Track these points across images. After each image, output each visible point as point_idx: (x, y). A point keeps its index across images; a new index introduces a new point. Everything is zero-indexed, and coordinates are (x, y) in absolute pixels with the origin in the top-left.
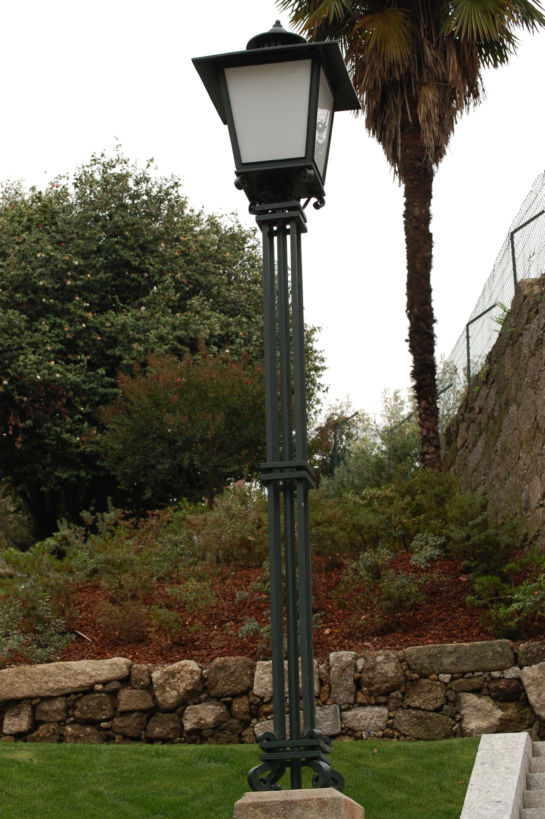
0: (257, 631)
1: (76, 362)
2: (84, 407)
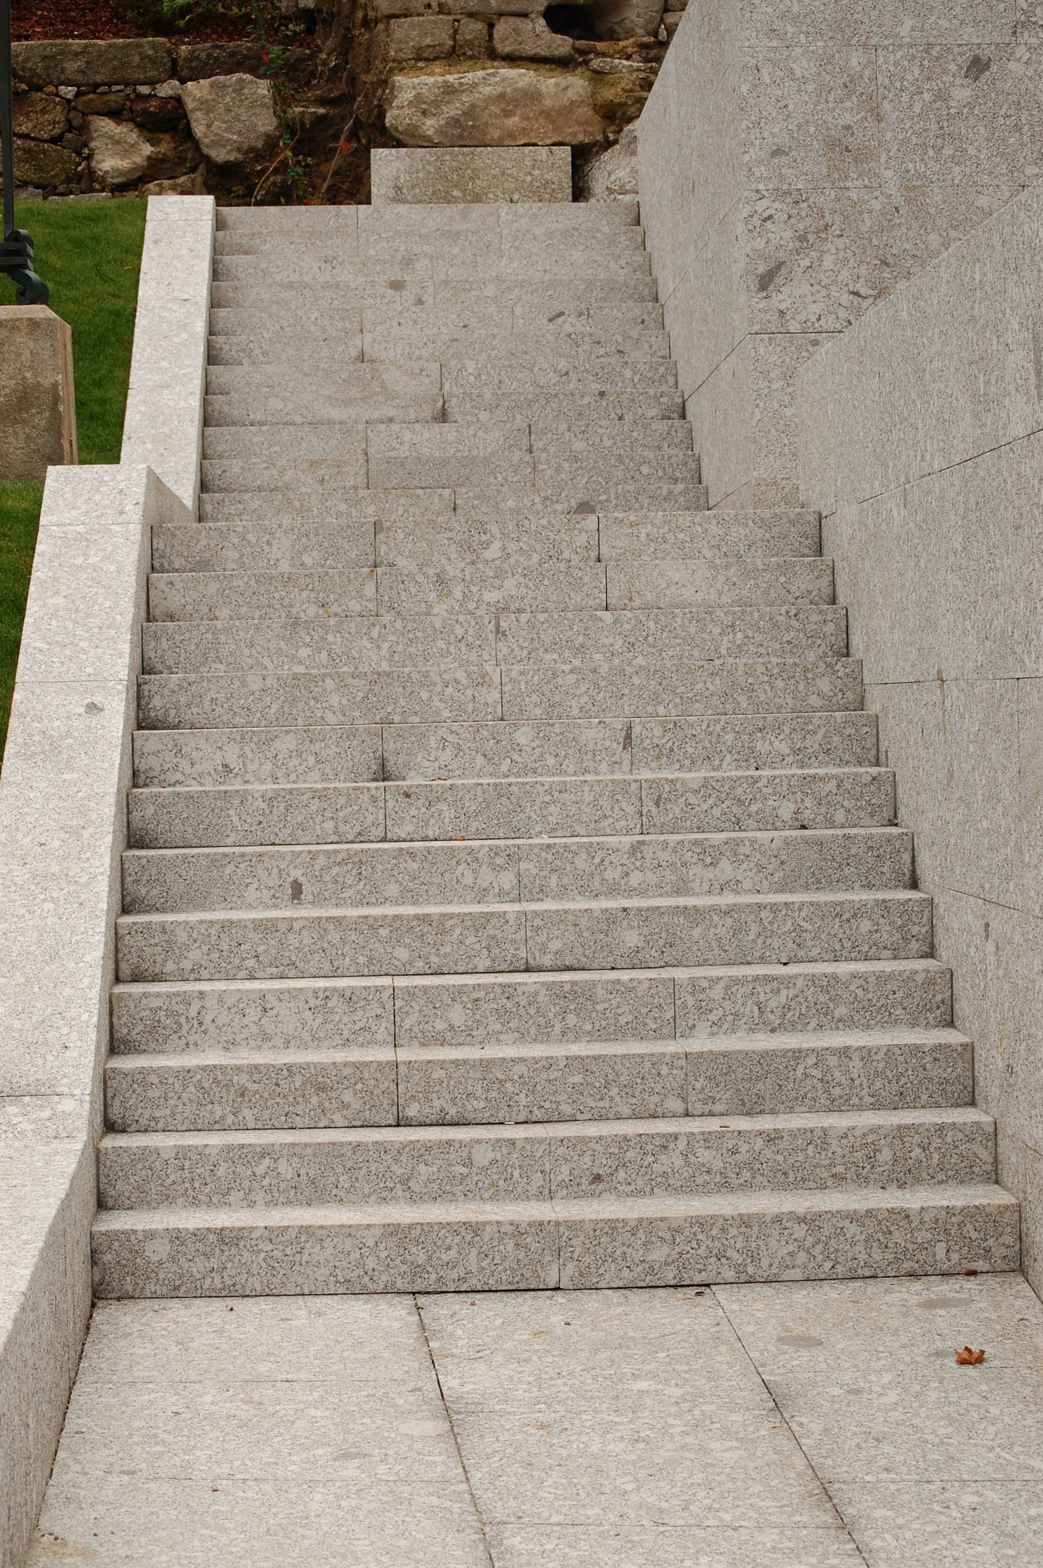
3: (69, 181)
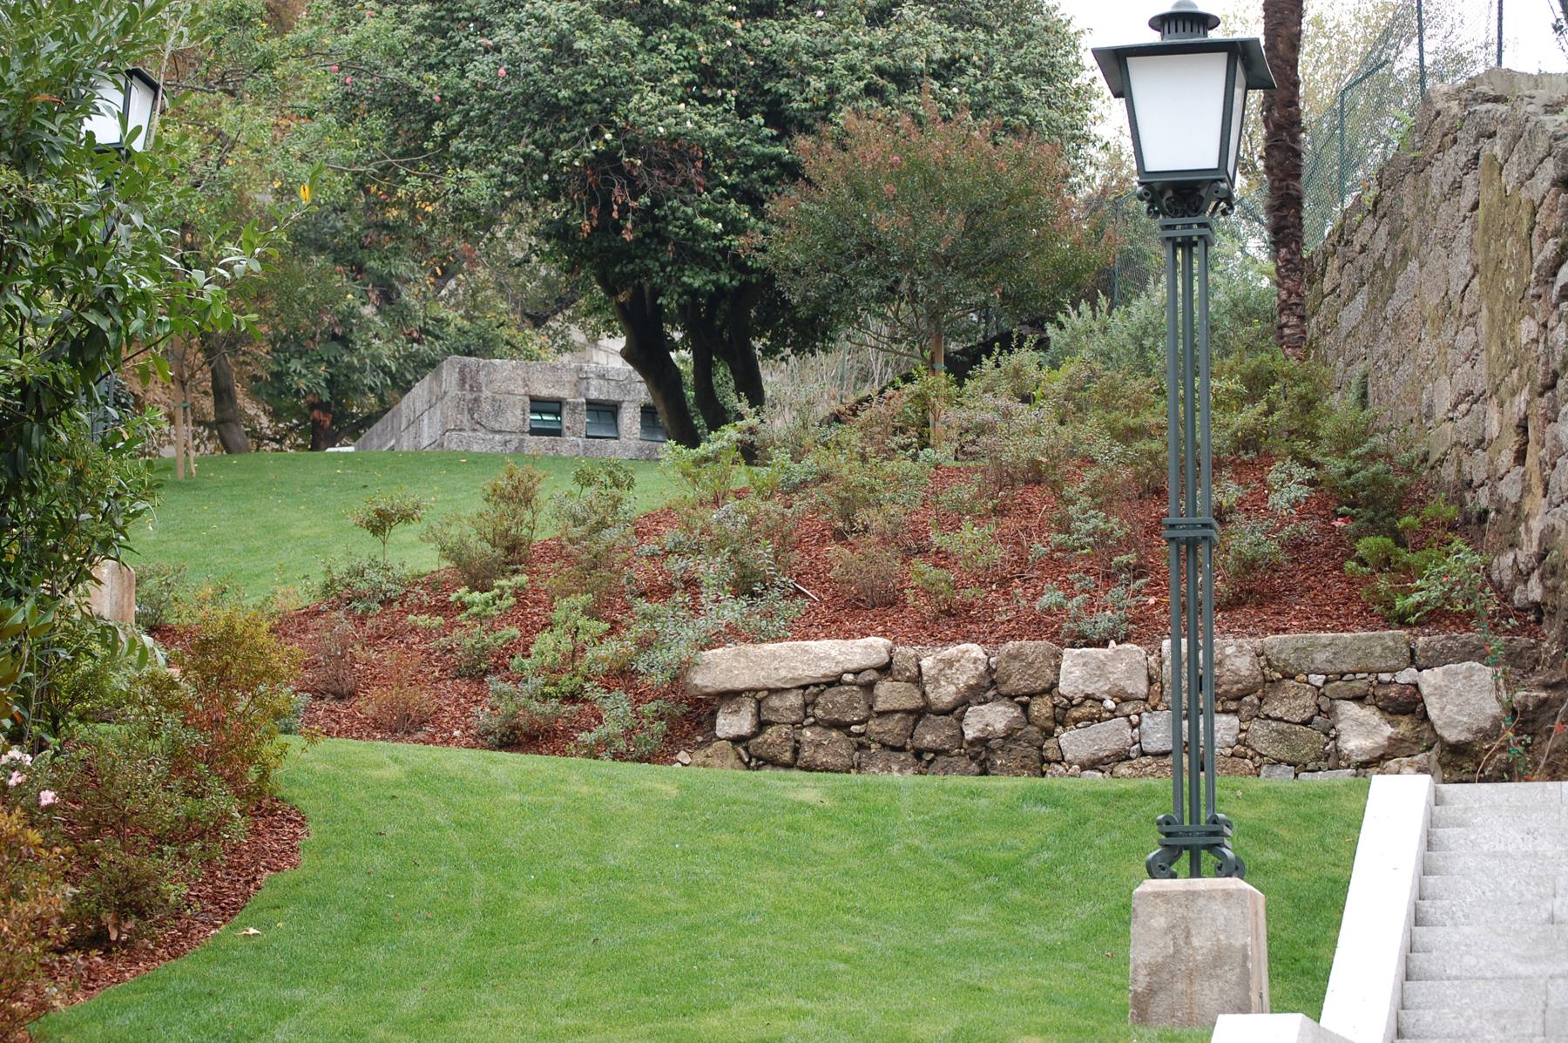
0: (1060, 607)
1: (717, 101)
2: (729, 175)
3: (1318, 759)
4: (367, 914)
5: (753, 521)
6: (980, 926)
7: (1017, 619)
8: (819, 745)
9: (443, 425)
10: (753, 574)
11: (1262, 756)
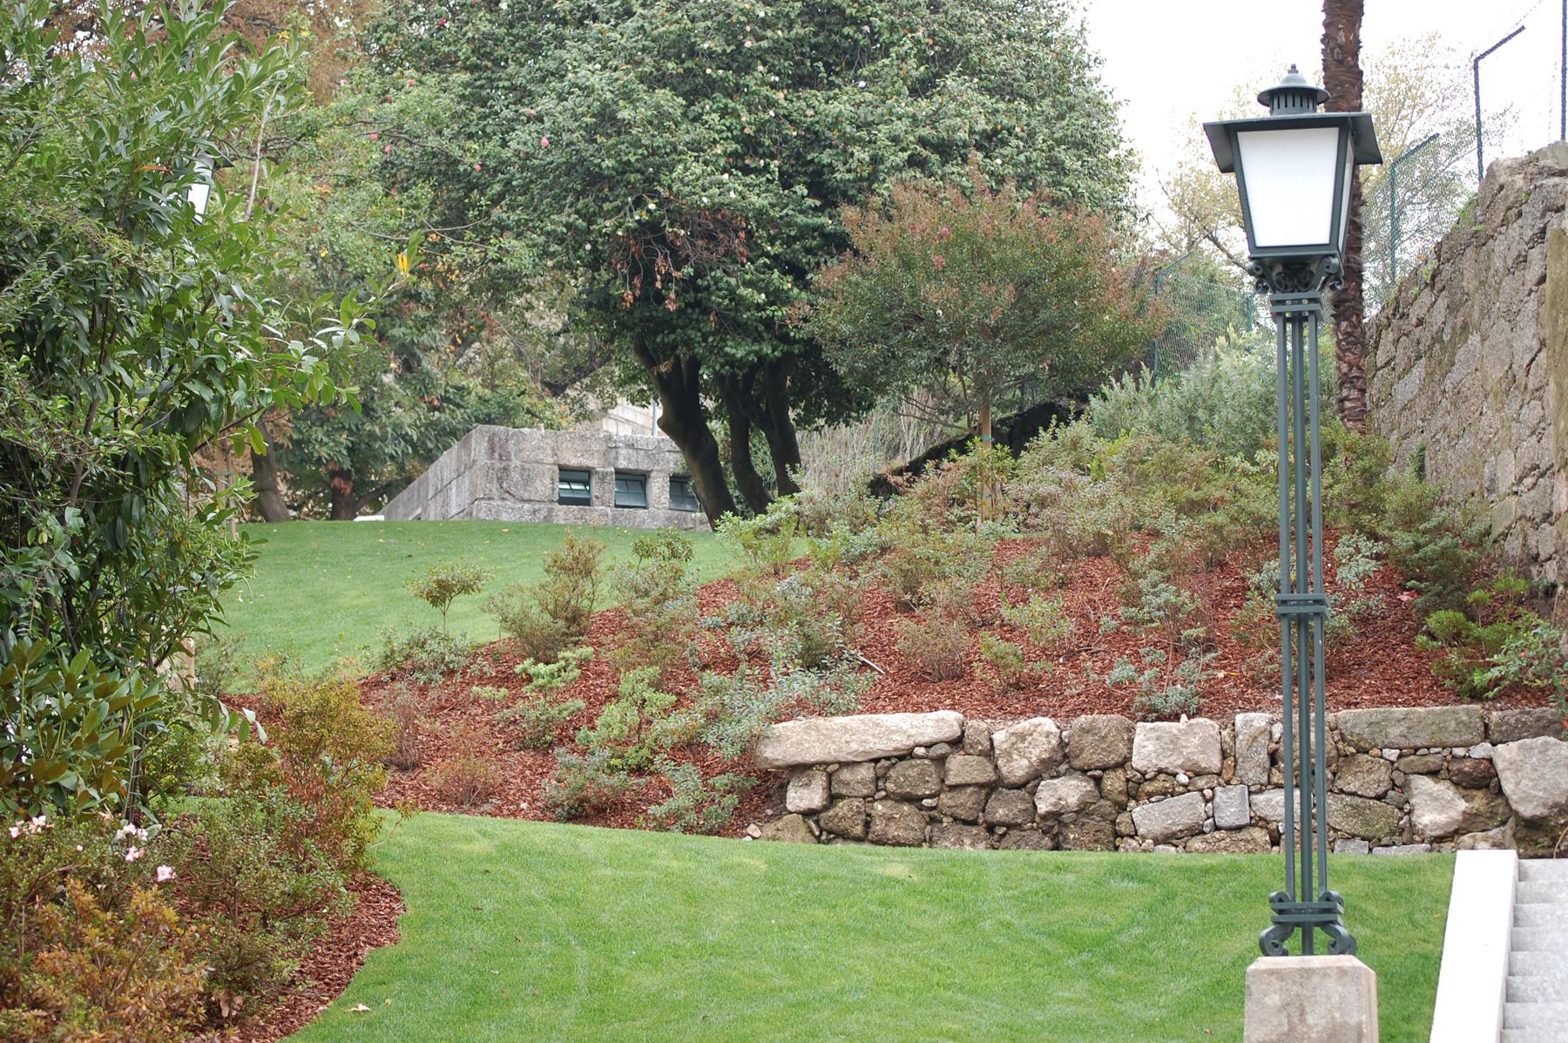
1: (758, 171)
2: (772, 245)
3: (1392, 833)
4: (474, 989)
5: (817, 593)
6: (1078, 1002)
7: (1087, 692)
8: (891, 818)
9: (472, 494)
10: (819, 646)
11: (1336, 830)
